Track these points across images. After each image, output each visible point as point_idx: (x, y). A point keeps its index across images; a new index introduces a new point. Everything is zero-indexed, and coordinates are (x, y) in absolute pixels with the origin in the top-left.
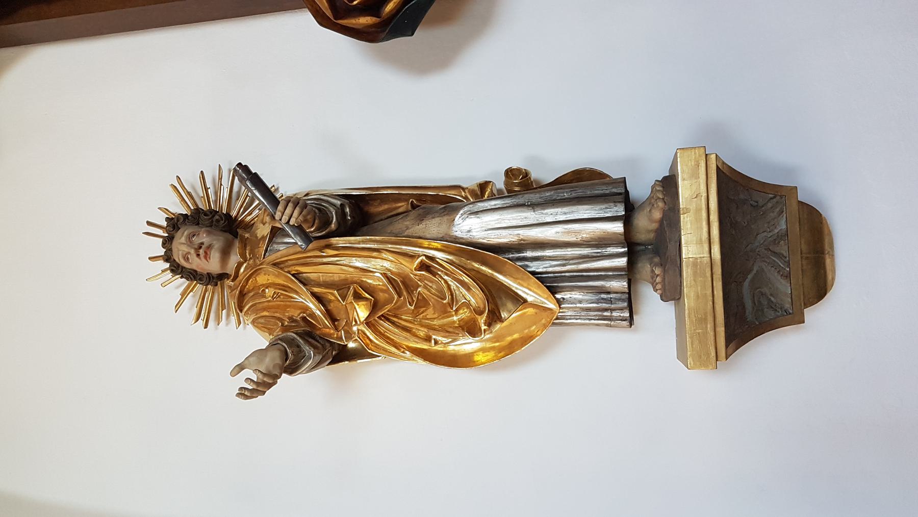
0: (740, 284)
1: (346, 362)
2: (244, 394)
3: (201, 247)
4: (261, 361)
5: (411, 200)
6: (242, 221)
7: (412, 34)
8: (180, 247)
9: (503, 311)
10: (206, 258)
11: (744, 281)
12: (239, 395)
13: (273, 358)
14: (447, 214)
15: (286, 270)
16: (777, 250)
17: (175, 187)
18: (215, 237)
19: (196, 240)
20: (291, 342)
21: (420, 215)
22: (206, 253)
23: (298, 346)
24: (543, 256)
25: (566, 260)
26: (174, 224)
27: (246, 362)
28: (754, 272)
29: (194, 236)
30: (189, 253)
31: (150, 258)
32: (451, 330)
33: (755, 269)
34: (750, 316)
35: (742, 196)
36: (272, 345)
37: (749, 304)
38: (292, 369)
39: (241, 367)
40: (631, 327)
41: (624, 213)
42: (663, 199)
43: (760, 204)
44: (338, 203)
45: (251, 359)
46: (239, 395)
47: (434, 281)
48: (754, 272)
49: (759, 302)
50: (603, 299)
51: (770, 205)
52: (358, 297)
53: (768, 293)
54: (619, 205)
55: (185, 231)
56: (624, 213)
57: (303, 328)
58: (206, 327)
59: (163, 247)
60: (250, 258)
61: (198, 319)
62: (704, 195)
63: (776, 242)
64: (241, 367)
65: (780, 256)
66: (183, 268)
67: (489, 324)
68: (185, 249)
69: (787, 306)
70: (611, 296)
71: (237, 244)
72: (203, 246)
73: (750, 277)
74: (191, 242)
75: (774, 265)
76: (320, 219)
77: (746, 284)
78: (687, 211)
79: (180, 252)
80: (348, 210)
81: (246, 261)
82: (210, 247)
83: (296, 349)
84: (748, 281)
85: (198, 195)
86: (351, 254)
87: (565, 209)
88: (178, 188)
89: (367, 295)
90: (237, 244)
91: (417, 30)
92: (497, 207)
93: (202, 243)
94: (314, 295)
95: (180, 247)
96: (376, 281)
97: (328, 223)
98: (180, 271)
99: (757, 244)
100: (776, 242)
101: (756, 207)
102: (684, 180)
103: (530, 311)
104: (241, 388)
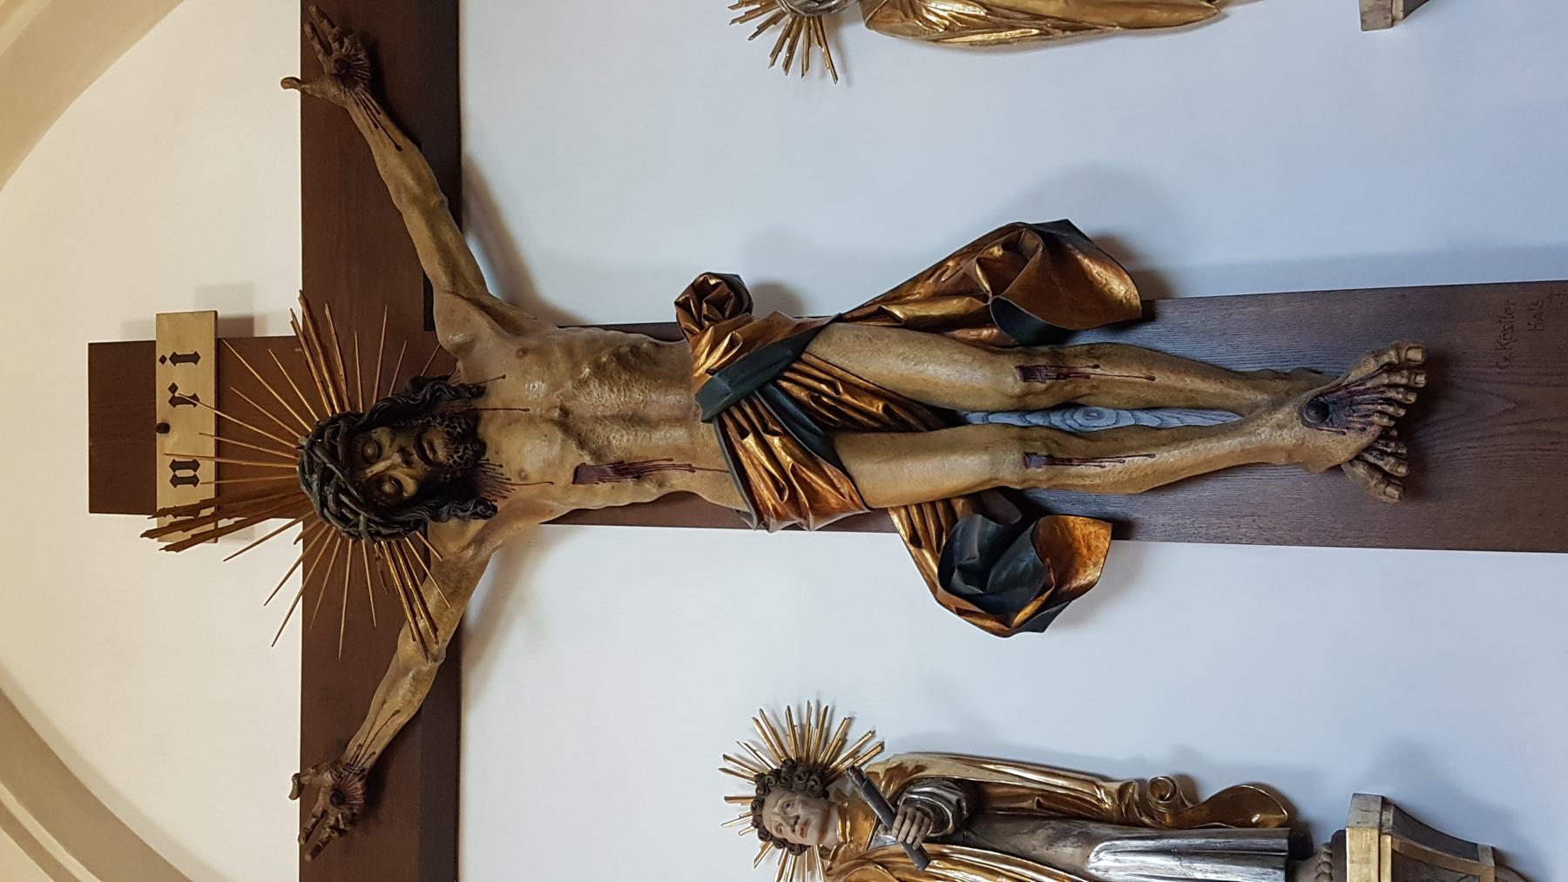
5: (1037, 798)
7: (1043, 631)
9: (1138, 307)
14: (1081, 846)
17: (757, 721)
18: (812, 810)
19: (792, 812)
21: (1049, 836)
22: (802, 830)
29: (788, 806)
30: (781, 824)
31: (727, 799)
42: (1330, 874)
44: (953, 798)
54: (1279, 872)
55: (780, 798)
60: (851, 841)
71: (835, 815)
74: (785, 813)
76: (934, 823)
79: (773, 823)
80: (964, 804)
81: (846, 842)
82: (806, 823)
86: (962, 854)
87: (1217, 867)
90: (835, 815)
91: (1050, 626)
92: (1138, 849)
97: (945, 823)
98: (769, 838)
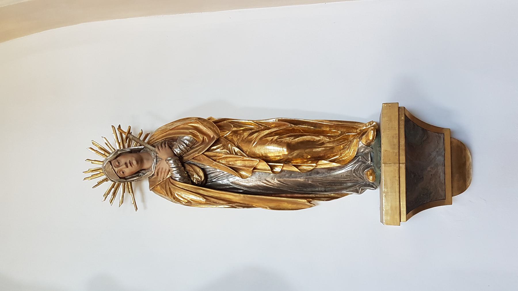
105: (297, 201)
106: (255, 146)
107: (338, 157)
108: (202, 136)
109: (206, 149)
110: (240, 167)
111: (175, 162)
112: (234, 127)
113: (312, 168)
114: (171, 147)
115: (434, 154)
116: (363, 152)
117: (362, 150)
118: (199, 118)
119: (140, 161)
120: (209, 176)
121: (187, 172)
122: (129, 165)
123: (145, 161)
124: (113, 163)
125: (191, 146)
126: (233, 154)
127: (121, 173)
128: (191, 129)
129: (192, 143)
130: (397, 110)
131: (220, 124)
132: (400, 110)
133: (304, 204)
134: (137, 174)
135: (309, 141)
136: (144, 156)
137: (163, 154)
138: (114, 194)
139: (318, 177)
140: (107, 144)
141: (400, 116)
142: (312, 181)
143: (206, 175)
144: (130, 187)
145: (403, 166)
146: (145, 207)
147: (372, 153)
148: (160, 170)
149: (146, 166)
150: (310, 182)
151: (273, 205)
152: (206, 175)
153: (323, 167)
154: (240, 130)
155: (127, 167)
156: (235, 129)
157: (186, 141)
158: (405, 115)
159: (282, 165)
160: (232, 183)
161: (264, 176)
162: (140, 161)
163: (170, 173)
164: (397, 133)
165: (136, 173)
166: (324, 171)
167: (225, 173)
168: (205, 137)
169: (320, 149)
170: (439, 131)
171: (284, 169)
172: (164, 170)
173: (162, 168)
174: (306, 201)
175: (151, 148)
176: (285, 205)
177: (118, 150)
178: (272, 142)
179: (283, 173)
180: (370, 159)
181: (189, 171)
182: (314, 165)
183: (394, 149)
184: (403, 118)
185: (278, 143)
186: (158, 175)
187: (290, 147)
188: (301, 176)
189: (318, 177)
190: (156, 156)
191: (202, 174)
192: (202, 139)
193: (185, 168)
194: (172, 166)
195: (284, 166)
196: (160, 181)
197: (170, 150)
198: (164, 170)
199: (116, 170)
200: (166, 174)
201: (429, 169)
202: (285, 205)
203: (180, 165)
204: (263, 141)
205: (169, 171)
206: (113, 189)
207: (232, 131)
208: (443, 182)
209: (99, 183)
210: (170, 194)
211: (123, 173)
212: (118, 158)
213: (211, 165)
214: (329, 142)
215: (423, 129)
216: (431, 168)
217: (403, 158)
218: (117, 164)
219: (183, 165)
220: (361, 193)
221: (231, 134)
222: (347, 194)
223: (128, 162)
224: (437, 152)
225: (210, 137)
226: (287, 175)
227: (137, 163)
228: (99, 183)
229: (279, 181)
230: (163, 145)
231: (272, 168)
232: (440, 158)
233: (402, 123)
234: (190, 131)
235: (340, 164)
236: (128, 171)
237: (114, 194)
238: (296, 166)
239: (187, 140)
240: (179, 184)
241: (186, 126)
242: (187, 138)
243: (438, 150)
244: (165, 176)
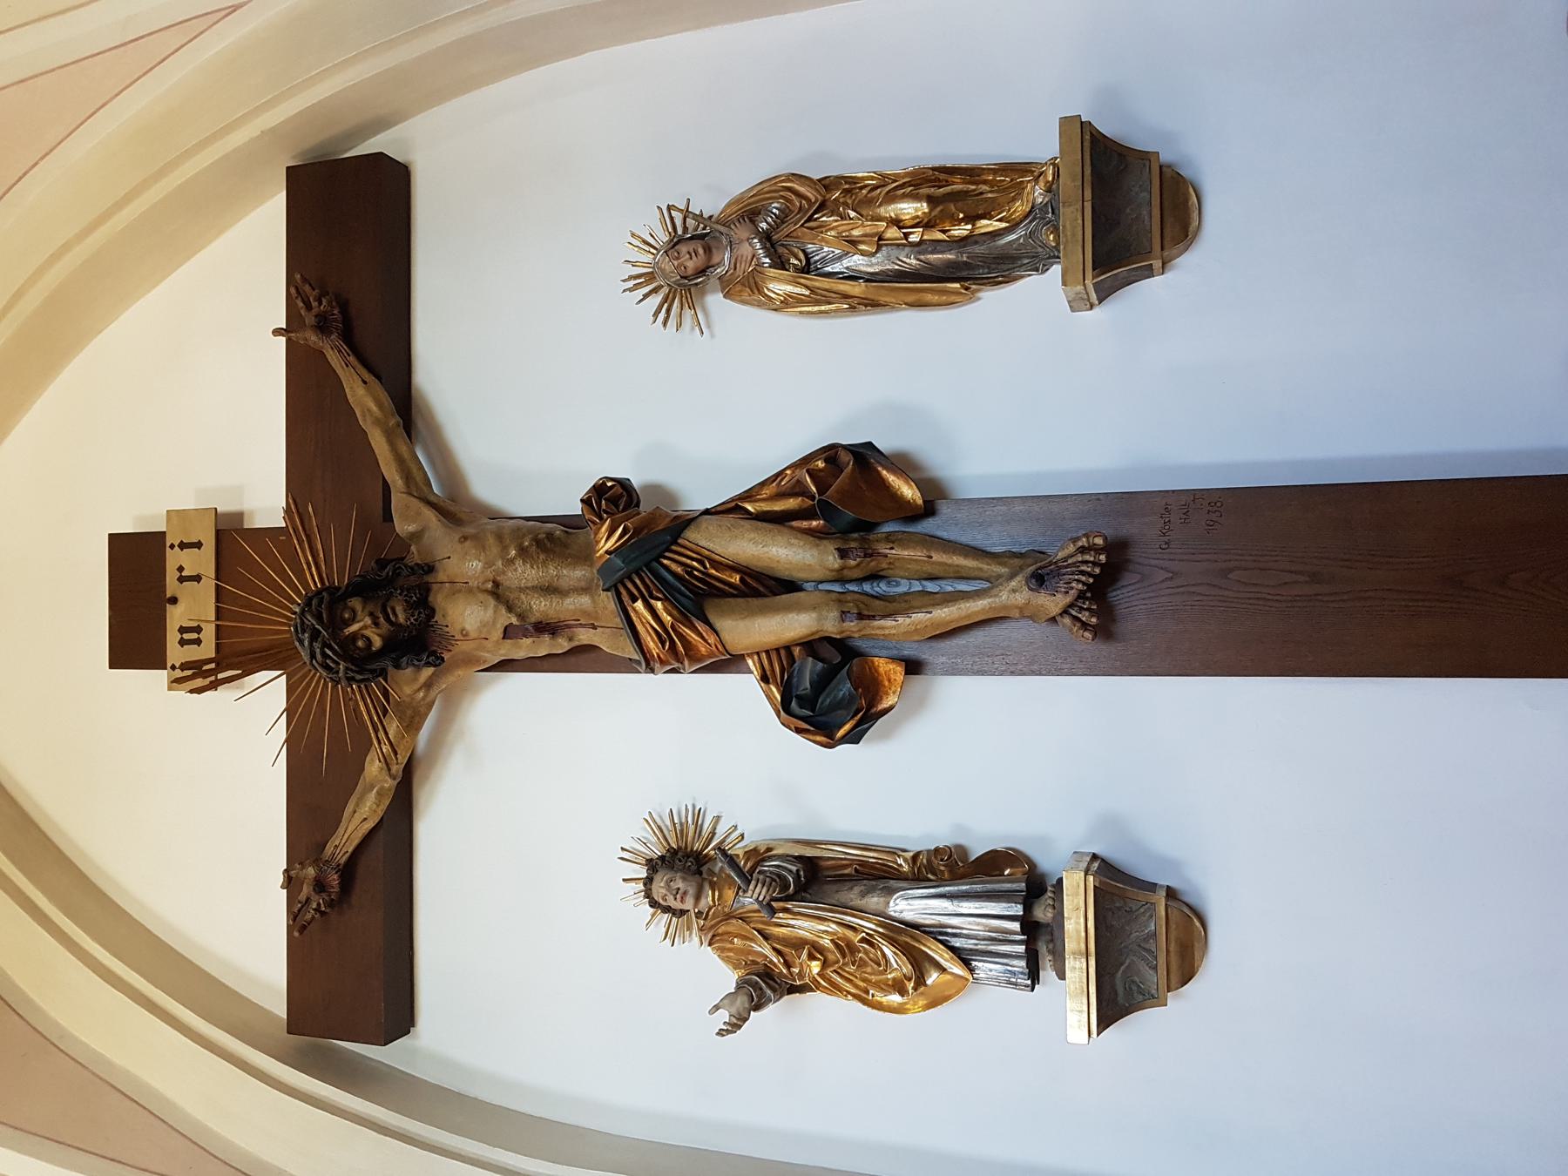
0: (1113, 975)
1: (798, 994)
2: (721, 1033)
3: (677, 893)
4: (732, 1003)
6: (706, 855)
8: (659, 889)
10: (682, 902)
11: (1117, 972)
12: (718, 1034)
13: (742, 1001)
15: (752, 925)
16: (1147, 946)
18: (689, 883)
19: (674, 885)
20: (755, 985)
22: (682, 898)
23: (761, 989)
24: (961, 933)
25: (978, 940)
26: (653, 865)
27: (721, 1003)
28: (1126, 965)
30: (666, 895)
32: (883, 986)
33: (1128, 961)
34: (1121, 999)
35: (1117, 905)
36: (739, 987)
37: (1120, 990)
38: (757, 1008)
39: (717, 1008)
40: (1033, 990)
41: (1021, 913)
43: (1134, 909)
44: (794, 869)
45: (725, 1001)
46: (718, 1034)
47: (895, 279)
48: (1126, 965)
49: (1131, 989)
50: (1009, 971)
51: (1142, 910)
52: (811, 957)
53: (1138, 981)
56: (1021, 913)
57: (761, 969)
58: (673, 945)
59: (651, 906)
61: (665, 938)
62: (1083, 909)
63: (1146, 940)
64: (717, 1008)
65: (1149, 951)
66: (659, 904)
67: (915, 989)
68: (664, 891)
69: (1154, 992)
70: (1015, 969)
71: (707, 887)
72: (680, 892)
73: (1123, 968)
75: (1144, 959)
77: (1119, 974)
78: (1069, 919)
80: (802, 873)
82: (685, 893)
83: (759, 992)
84: (1120, 972)
85: (667, 827)
88: (651, 821)
89: (819, 956)
90: (707, 887)
93: (679, 889)
94: (774, 949)
95: (659, 889)
96: (826, 942)
99: (1130, 941)
100: (1146, 940)
101: (1131, 911)
102: (1067, 895)
103: (948, 977)
104: (720, 1030)
105: (946, 287)
106: (880, 205)
107: (1005, 214)
108: (799, 199)
109: (806, 218)
110: (859, 239)
111: (760, 241)
112: (846, 183)
113: (966, 233)
114: (753, 222)
115: (1136, 189)
116: (1041, 203)
117: (1040, 200)
118: (793, 174)
119: (708, 250)
120: (812, 260)
121: (780, 257)
122: (693, 254)
123: (714, 250)
124: (669, 253)
125: (782, 218)
126: (846, 219)
127: (683, 268)
128: (782, 191)
129: (783, 213)
130: (1079, 125)
131: (823, 182)
132: (1084, 125)
133: (955, 292)
134: (702, 272)
135: (959, 192)
136: (713, 244)
137: (742, 232)
138: (668, 311)
139: (978, 249)
140: (652, 236)
141: (1084, 134)
142: (968, 257)
143: (808, 259)
144: (690, 301)
145: (1088, 206)
146: (712, 336)
147: (1053, 202)
148: (739, 258)
149: (715, 260)
150: (965, 259)
151: (911, 298)
152: (808, 259)
153: (983, 231)
154: (855, 188)
155: (691, 258)
156: (847, 186)
157: (774, 211)
158: (1091, 133)
159: (921, 230)
160: (847, 268)
161: (894, 252)
162: (708, 250)
163: (755, 259)
164: (1080, 157)
165: (701, 272)
166: (984, 238)
167: (837, 252)
168: (804, 202)
169: (1013, 237)
170: (1145, 157)
171: (925, 237)
172: (744, 258)
173: (742, 256)
174: (958, 285)
175: (722, 229)
176: (929, 297)
177: (654, 259)
178: (904, 197)
179: (923, 247)
180: (1050, 210)
181: (783, 253)
182: (969, 227)
183: (1073, 181)
184: (1087, 137)
185: (915, 197)
186: (735, 269)
187: (931, 200)
188: (951, 250)
189: (978, 249)
190: (731, 241)
191: (802, 256)
192: (798, 204)
193: (776, 251)
194: (758, 247)
195: (925, 232)
196: (739, 276)
197: (751, 225)
198: (744, 258)
199: (676, 263)
200: (748, 265)
201: (1128, 211)
202: (929, 297)
203: (768, 245)
204: (891, 198)
205: (754, 256)
206: (666, 305)
207: (844, 189)
208: (1148, 228)
209: (646, 296)
210: (756, 291)
211: (685, 268)
212: (676, 248)
213: (815, 241)
214: (990, 192)
215: (1120, 155)
216: (1131, 209)
217: (1088, 194)
218: (676, 254)
219: (773, 245)
220: (1044, 272)
221: (842, 195)
222: (1022, 277)
223: (691, 251)
224: (1141, 186)
225: (811, 200)
226: (930, 249)
227: (705, 252)
228: (646, 296)
229: (918, 260)
230: (741, 220)
231: (906, 235)
232: (1145, 194)
233: (1087, 144)
234: (781, 193)
235: (1000, 220)
236: (691, 265)
237: (668, 311)
238: (944, 232)
239: (776, 208)
240: (770, 272)
241: (773, 188)
242: (775, 207)
243: (1141, 183)
244: (747, 267)
